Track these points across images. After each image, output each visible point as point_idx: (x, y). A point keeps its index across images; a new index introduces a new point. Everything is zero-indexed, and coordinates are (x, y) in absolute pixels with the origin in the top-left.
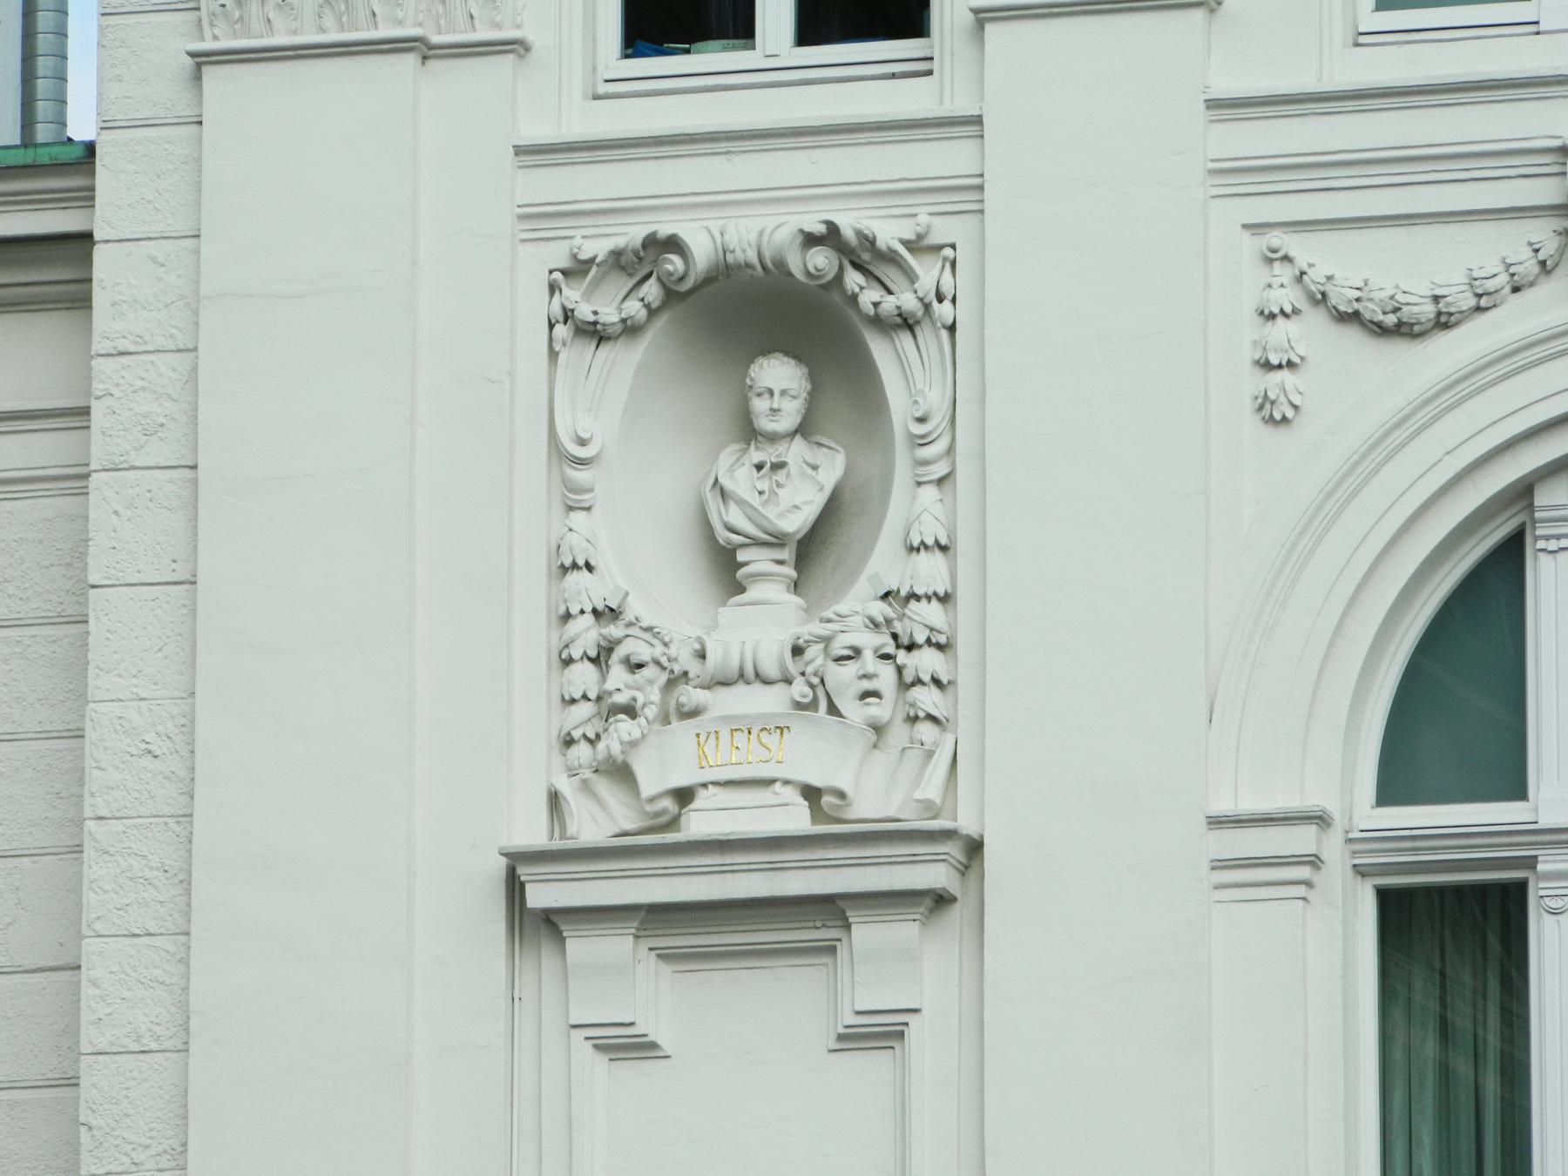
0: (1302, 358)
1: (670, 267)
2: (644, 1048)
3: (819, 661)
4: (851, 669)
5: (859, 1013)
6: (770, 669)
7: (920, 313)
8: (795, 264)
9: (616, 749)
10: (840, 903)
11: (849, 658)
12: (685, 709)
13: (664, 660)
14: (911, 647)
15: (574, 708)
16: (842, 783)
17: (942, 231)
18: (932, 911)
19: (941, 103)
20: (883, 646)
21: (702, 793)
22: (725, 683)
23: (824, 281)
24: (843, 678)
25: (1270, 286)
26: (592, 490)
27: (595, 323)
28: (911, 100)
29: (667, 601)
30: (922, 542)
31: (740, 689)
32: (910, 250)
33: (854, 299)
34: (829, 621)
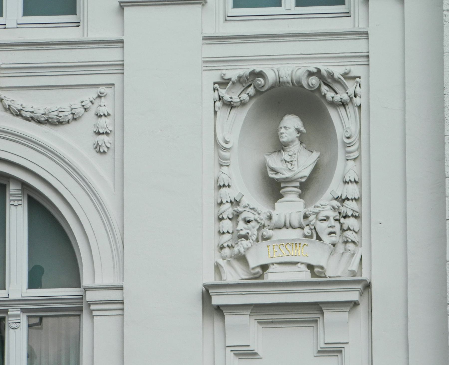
0: (110, 131)
1: (259, 82)
2: (252, 354)
3: (314, 221)
4: (325, 224)
5: (326, 344)
6: (295, 223)
7: (348, 101)
8: (304, 83)
9: (242, 250)
10: (321, 305)
11: (325, 220)
12: (265, 237)
13: (258, 219)
14: (345, 217)
15: (224, 236)
16: (323, 264)
17: (355, 71)
18: (351, 308)
19: (83, 36)
20: (337, 216)
21: (272, 266)
22: (280, 228)
23: (313, 89)
24: (322, 227)
25: (100, 106)
26: (229, 159)
27: (231, 101)
28: (344, 25)
29: (254, 200)
30: (350, 180)
31: (284, 230)
32: (345, 78)
33: (324, 96)
34: (318, 207)
